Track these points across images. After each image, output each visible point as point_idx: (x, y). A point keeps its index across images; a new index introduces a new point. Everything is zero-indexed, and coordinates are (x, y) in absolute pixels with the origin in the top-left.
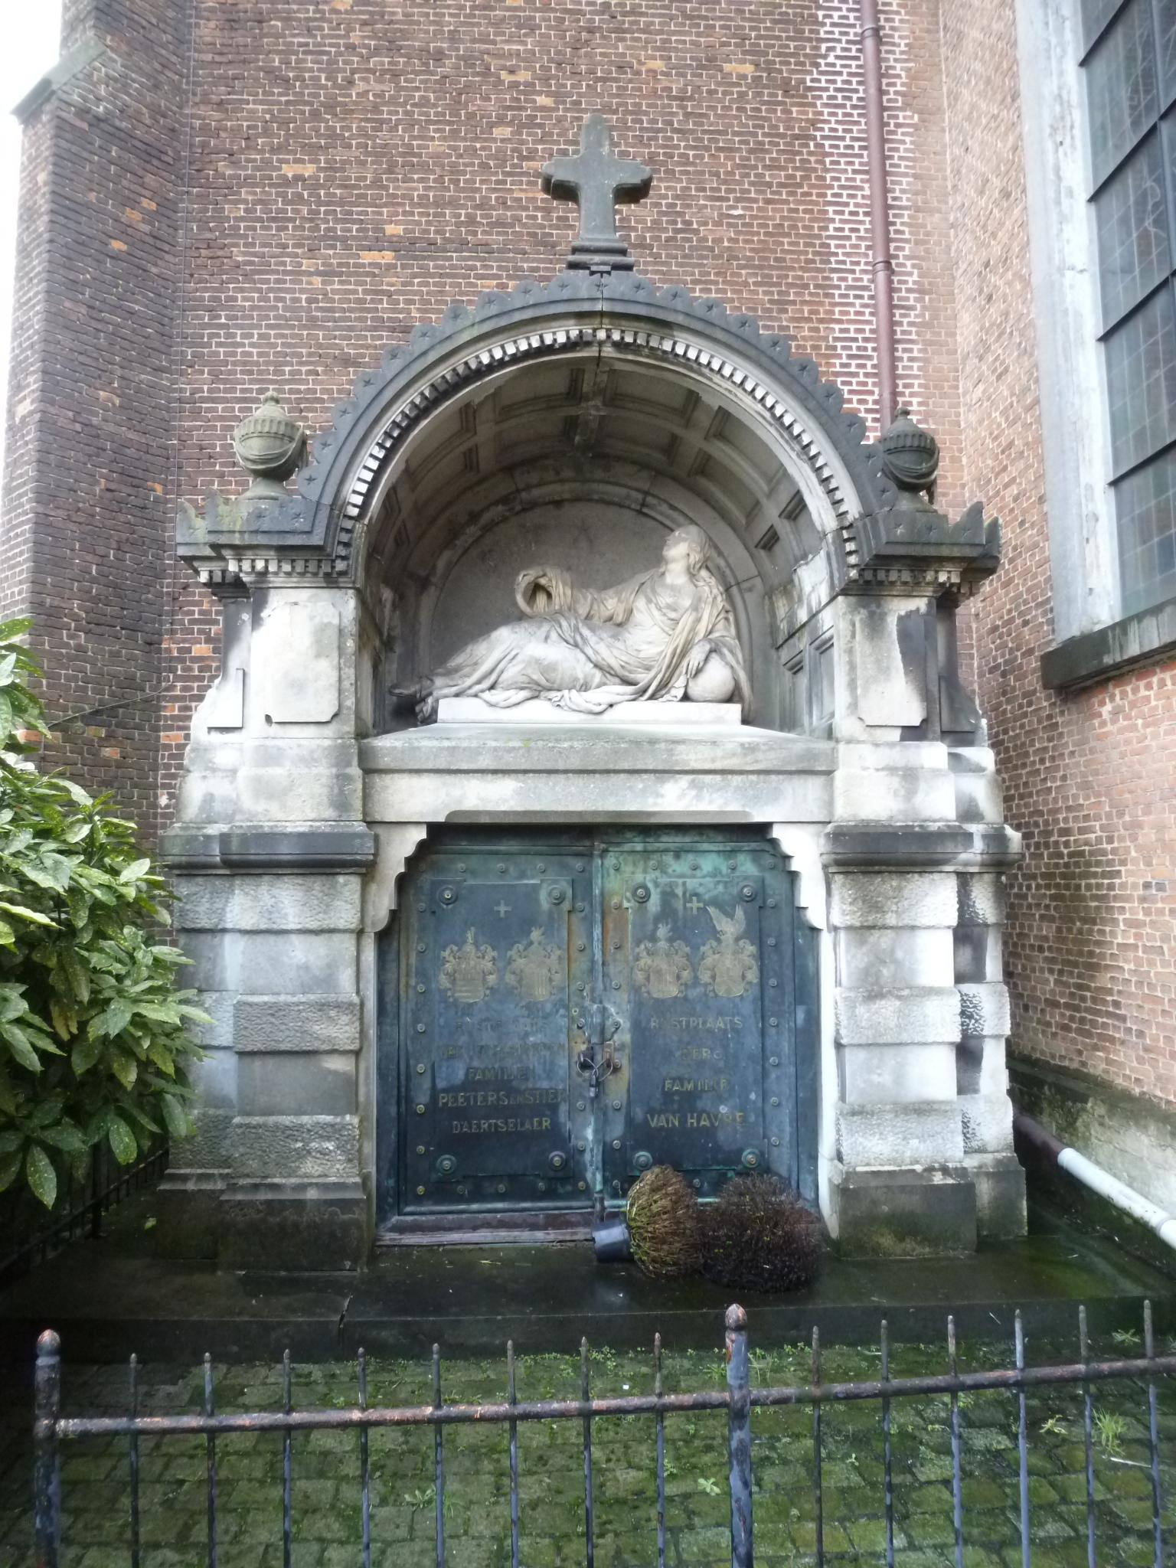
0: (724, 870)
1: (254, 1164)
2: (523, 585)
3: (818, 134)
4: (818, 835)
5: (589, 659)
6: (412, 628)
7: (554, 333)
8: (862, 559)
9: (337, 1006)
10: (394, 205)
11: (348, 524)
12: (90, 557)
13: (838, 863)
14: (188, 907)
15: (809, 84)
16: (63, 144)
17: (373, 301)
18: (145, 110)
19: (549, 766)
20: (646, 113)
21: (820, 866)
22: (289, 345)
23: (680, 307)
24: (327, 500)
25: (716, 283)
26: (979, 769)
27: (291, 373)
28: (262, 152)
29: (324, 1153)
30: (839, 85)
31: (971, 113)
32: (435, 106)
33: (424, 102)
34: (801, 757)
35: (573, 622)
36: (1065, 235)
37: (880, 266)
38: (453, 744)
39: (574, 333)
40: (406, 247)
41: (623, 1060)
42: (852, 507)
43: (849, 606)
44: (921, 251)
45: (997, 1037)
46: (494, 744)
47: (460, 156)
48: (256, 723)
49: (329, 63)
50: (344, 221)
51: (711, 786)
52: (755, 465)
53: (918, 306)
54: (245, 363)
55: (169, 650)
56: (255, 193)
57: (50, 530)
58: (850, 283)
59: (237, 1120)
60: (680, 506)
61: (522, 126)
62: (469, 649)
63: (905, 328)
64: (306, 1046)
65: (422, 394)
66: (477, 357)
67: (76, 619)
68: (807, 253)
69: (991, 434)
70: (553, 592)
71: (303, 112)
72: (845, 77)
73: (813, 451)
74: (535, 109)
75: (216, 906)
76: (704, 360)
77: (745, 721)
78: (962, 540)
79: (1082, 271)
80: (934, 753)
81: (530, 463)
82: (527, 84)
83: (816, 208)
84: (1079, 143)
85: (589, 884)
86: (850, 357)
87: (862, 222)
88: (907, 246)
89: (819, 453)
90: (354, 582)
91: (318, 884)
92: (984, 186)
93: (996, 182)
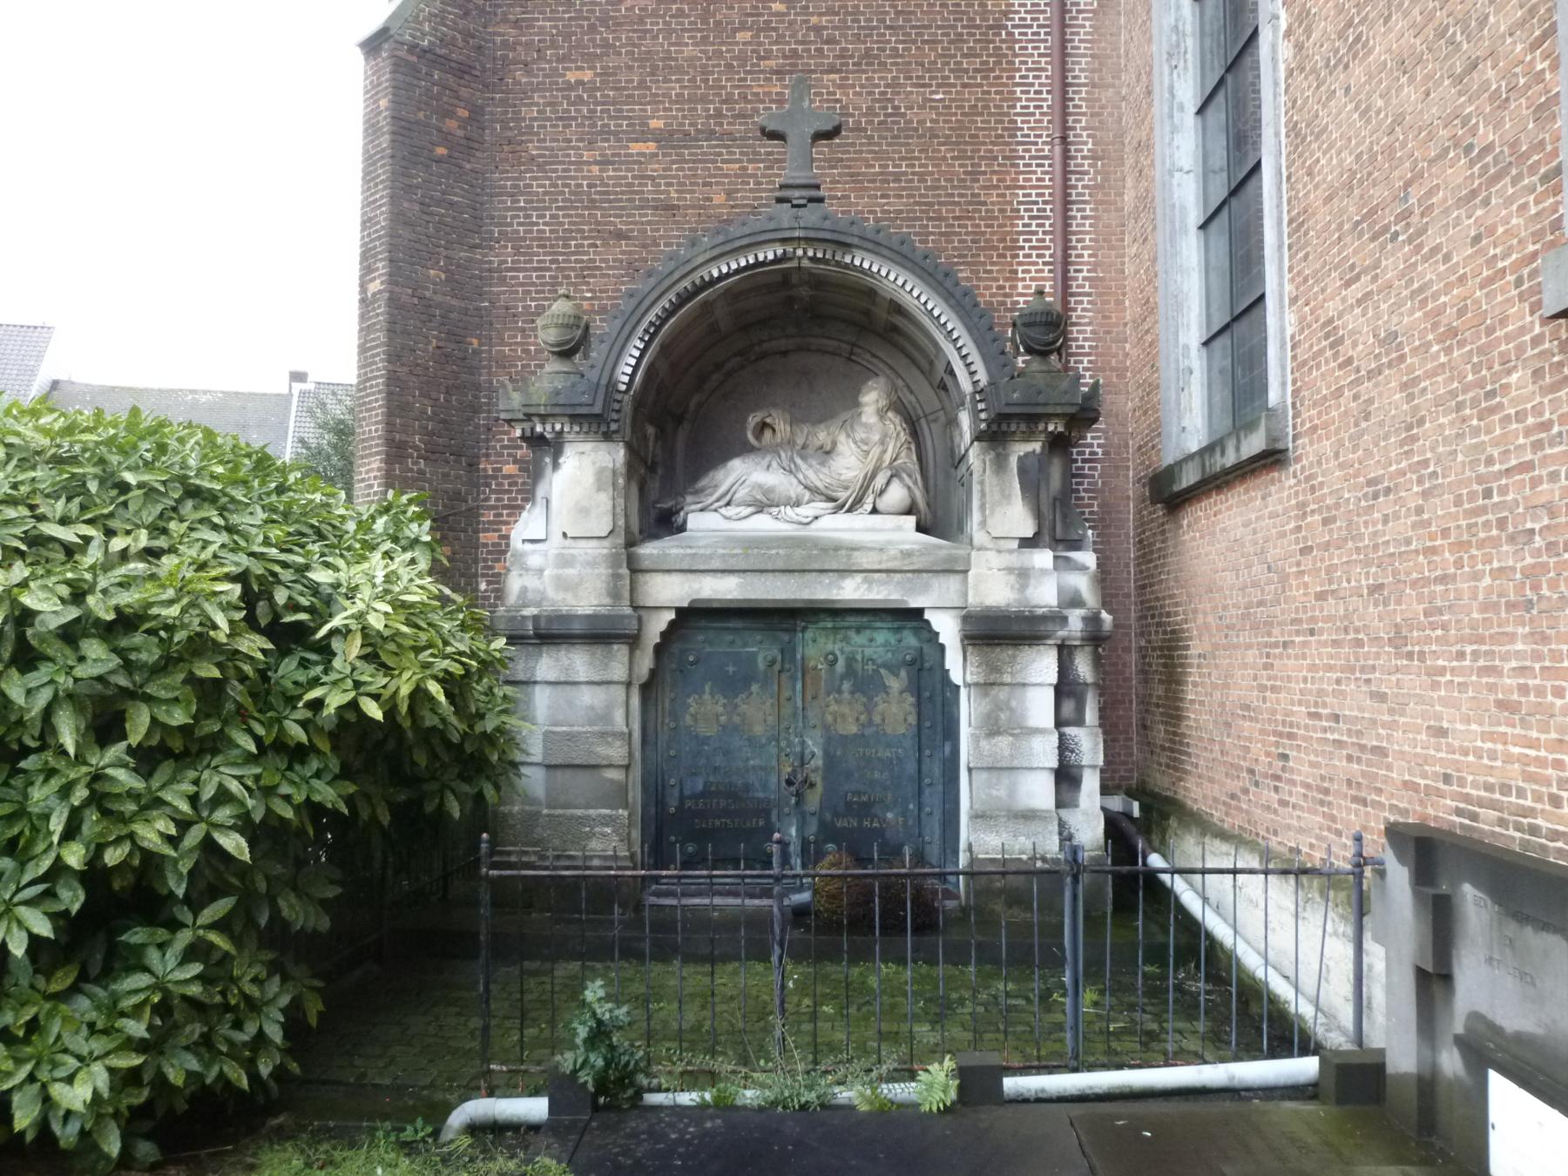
1: (557, 842)
9: (614, 734)
11: (619, 397)
16: (401, 77)
17: (640, 185)
20: (863, 13)
23: (856, 232)
24: (604, 382)
25: (919, 159)
26: (1084, 568)
28: (550, 62)
29: (604, 835)
32: (688, 16)
36: (1176, 143)
37: (1057, 141)
39: (780, 252)
40: (664, 138)
41: (817, 778)
42: (982, 377)
45: (1093, 767)
47: (709, 59)
48: (556, 538)
50: (617, 118)
54: (541, 239)
55: (485, 470)
59: (545, 811)
60: (880, 354)
61: (760, 30)
62: (711, 474)
64: (592, 762)
67: (417, 448)
71: (582, 27)
73: (955, 335)
74: (771, 14)
80: (1043, 558)
84: (1190, 65)
85: (794, 650)
86: (1031, 218)
87: (1045, 100)
91: (599, 651)
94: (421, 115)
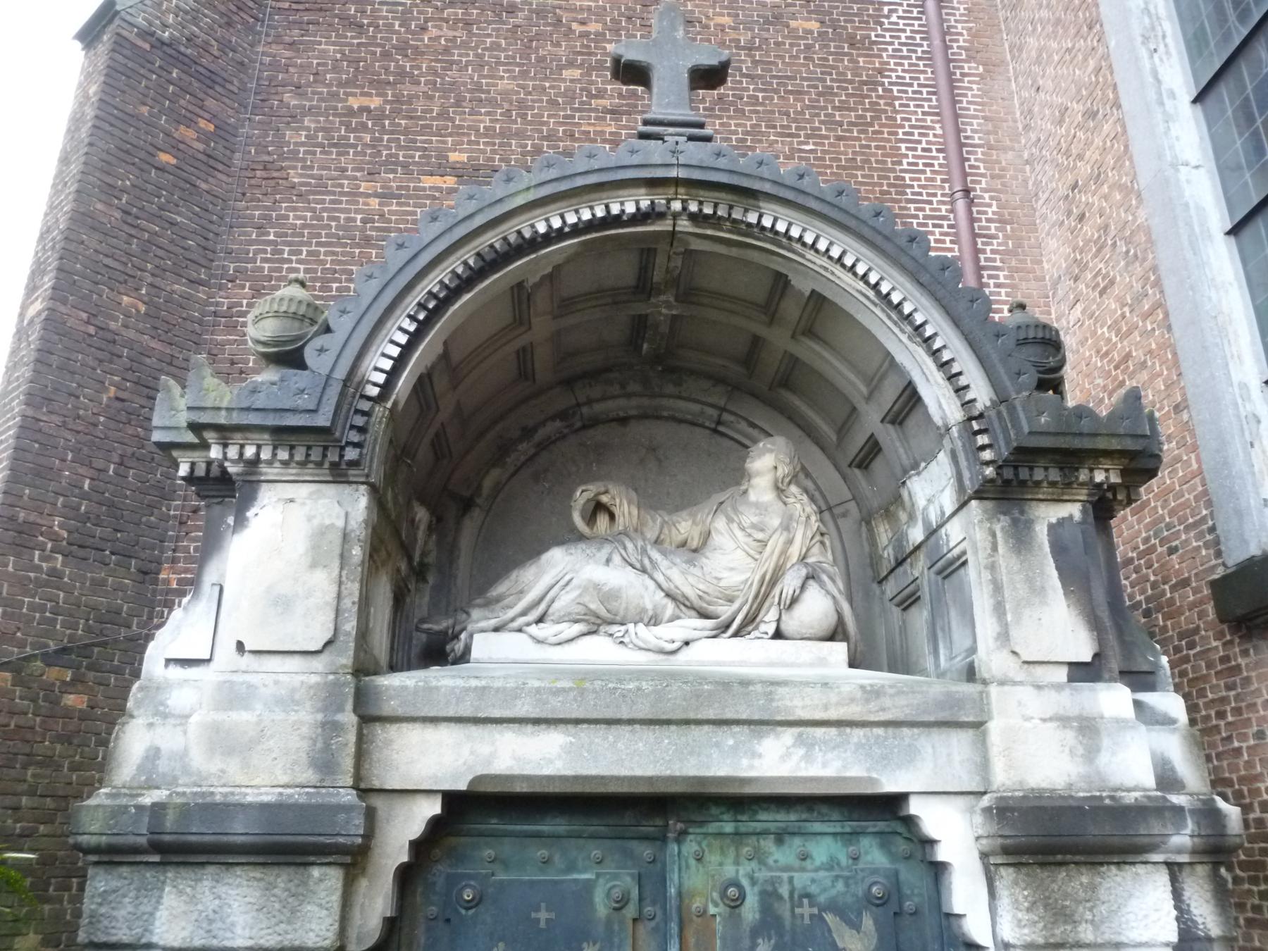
0: (844, 860)
2: (581, 501)
3: (886, 81)
4: (971, 811)
5: (660, 586)
6: (450, 551)
7: (622, 203)
8: (999, 453)
10: (458, 134)
11: (365, 405)
12: (82, 470)
13: (1006, 851)
14: (103, 910)
15: (874, 38)
16: (120, 58)
18: (214, 43)
19: (609, 714)
21: (976, 855)
22: (340, 262)
24: (341, 373)
26: (1166, 721)
27: (338, 289)
28: (330, 85)
30: (903, 40)
31: (1039, 55)
32: (505, 50)
33: (496, 47)
34: (940, 705)
35: (640, 543)
36: (1173, 133)
38: (483, 683)
39: (645, 204)
42: (981, 394)
43: (985, 511)
44: (998, 184)
46: (537, 684)
47: (530, 93)
48: (226, 650)
49: (403, 13)
50: (409, 148)
51: (825, 742)
52: (853, 366)
53: (1000, 235)
55: (167, 581)
56: (319, 122)
57: (38, 436)
58: (928, 212)
62: (514, 575)
63: (989, 255)
65: (465, 263)
66: (532, 226)
67: (55, 539)
68: (881, 185)
69: (1098, 352)
70: (617, 511)
72: (908, 34)
73: (929, 331)
75: (142, 908)
76: (795, 232)
77: (853, 664)
78: (1122, 431)
79: (1197, 167)
81: (592, 375)
82: (597, 34)
83: (888, 145)
84: (1173, 51)
85: (663, 880)
88: (984, 180)
89: (936, 334)
90: (367, 476)
91: (282, 879)
92: (1062, 115)
93: (1078, 108)
94: (145, 110)
